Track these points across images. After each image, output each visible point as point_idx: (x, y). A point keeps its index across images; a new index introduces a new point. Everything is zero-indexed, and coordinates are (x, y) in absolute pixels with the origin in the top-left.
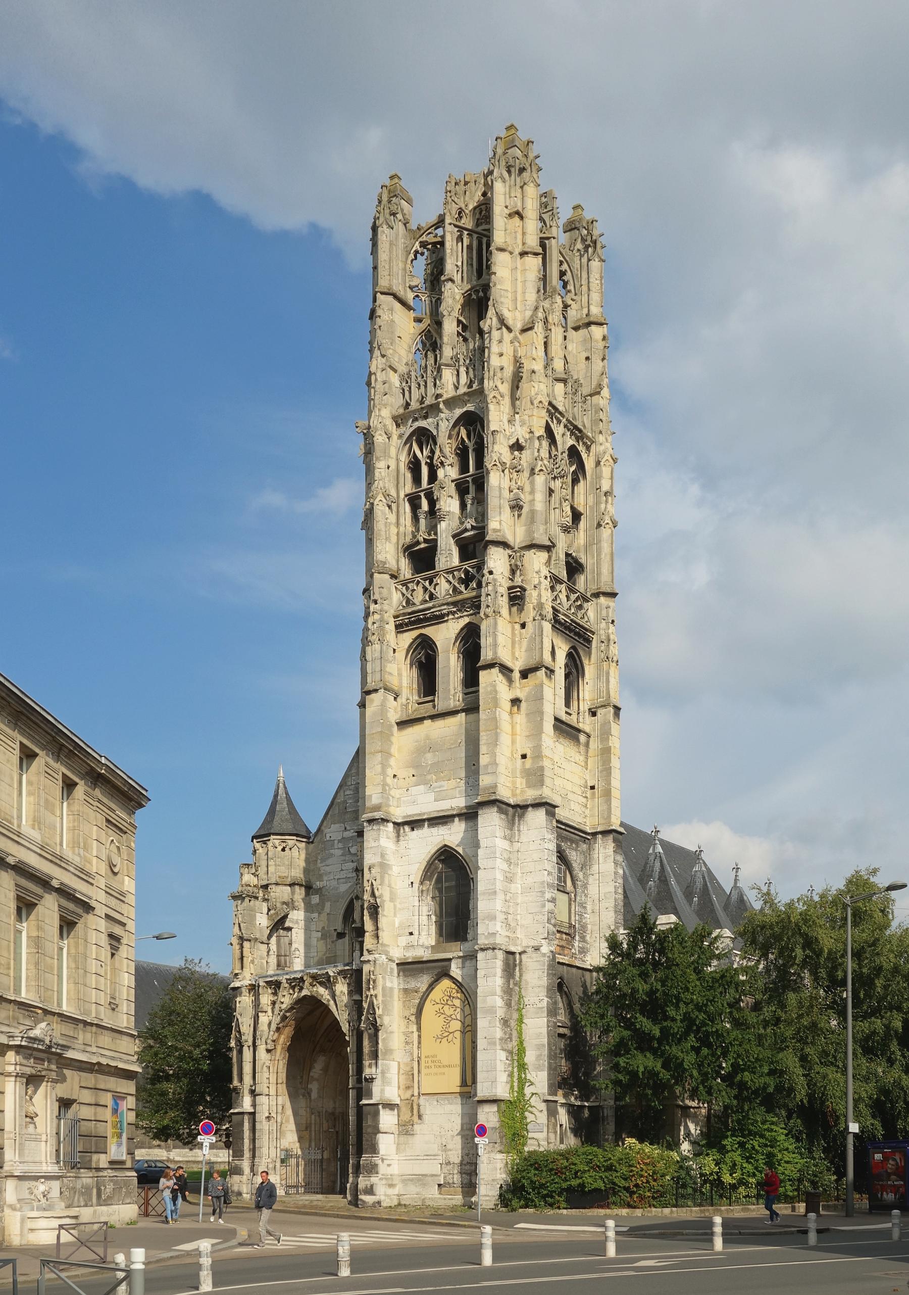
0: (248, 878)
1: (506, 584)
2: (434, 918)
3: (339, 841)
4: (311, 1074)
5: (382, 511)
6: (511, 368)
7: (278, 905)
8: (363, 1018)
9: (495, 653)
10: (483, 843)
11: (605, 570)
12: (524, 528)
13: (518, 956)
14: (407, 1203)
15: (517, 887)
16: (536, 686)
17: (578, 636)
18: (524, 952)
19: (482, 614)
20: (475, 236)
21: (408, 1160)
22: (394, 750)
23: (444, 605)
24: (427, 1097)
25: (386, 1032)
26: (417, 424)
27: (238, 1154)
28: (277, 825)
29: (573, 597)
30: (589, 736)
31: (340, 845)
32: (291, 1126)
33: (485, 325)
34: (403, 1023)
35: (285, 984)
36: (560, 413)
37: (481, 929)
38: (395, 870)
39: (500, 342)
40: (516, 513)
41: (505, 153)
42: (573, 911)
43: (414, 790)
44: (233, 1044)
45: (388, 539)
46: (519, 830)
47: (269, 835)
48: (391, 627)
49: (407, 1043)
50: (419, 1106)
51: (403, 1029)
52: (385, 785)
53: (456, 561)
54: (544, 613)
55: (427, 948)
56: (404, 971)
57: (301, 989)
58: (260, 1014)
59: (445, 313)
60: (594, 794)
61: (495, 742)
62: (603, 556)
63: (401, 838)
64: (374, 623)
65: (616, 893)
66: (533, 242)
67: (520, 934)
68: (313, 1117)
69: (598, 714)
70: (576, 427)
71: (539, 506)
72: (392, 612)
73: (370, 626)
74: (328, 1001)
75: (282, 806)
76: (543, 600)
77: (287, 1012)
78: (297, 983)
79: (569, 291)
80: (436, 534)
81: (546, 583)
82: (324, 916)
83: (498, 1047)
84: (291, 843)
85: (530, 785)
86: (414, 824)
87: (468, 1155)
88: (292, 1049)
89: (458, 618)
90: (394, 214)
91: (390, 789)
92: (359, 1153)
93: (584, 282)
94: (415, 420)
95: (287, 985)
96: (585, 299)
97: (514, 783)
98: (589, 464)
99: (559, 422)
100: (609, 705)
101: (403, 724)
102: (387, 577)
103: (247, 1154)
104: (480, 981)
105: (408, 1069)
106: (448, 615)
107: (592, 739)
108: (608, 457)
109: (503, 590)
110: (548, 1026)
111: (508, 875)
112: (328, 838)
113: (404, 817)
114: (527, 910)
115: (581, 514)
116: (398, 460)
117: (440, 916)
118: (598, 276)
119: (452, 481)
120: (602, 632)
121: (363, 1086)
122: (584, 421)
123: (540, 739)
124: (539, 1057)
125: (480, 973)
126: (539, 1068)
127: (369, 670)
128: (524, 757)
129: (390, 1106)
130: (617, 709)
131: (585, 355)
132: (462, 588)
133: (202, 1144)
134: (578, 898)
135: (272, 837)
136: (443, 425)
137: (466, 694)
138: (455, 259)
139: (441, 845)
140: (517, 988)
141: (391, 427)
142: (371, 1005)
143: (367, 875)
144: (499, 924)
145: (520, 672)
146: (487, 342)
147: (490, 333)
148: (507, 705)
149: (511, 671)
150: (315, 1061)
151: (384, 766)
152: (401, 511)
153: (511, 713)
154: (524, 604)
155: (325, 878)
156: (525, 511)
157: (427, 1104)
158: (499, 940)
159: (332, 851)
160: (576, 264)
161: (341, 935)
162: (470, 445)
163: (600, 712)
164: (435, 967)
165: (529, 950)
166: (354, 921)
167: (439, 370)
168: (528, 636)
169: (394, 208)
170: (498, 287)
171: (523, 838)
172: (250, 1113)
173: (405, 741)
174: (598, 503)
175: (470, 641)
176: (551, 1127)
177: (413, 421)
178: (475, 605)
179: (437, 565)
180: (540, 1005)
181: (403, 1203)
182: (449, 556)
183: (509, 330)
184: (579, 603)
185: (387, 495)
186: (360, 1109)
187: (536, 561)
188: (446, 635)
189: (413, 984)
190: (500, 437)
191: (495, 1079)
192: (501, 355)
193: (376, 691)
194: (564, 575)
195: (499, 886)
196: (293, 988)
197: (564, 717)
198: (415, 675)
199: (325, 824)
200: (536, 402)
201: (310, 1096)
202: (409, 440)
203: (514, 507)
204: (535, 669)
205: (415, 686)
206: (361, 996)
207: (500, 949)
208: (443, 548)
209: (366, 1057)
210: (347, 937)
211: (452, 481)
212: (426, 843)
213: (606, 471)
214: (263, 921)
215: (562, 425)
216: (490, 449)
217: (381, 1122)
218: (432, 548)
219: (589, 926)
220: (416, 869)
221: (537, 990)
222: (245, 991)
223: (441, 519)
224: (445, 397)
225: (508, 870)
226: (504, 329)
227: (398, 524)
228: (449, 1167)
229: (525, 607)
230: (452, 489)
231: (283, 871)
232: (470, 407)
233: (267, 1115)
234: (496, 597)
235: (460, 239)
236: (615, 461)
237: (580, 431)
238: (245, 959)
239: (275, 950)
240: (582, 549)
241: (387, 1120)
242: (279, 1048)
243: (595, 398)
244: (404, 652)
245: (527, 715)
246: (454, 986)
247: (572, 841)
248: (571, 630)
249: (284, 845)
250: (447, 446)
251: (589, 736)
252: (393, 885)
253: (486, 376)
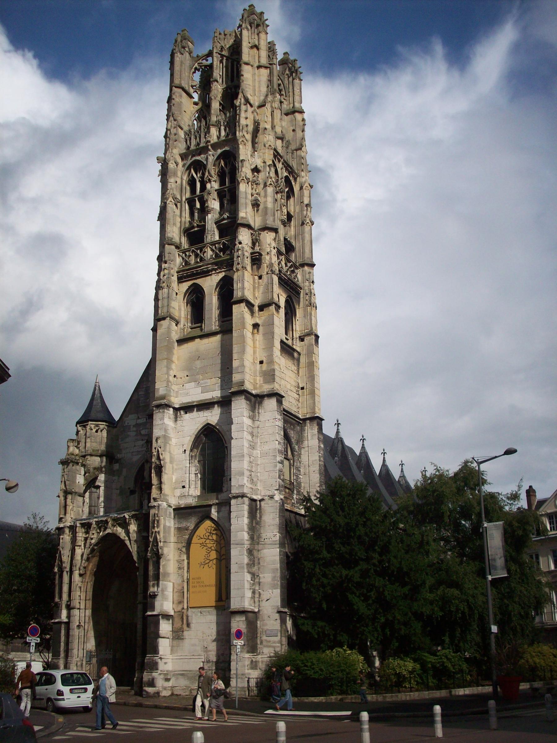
0: (73, 449)
1: (250, 251)
2: (199, 475)
3: (134, 426)
5: (171, 208)
6: (252, 126)
7: (91, 470)
8: (149, 549)
9: (243, 293)
10: (235, 420)
11: (307, 251)
12: (260, 218)
13: (258, 503)
14: (178, 693)
15: (257, 453)
17: (292, 289)
19: (234, 269)
20: (230, 61)
21: (178, 659)
22: (175, 358)
25: (165, 559)
26: (194, 158)
27: (56, 655)
28: (93, 415)
31: (135, 429)
32: (91, 634)
33: (237, 102)
34: (177, 553)
35: (94, 525)
36: (280, 156)
37: (233, 482)
38: (173, 441)
39: (246, 111)
41: (248, 17)
42: (292, 473)
43: (187, 386)
44: (56, 570)
45: (174, 224)
46: (259, 413)
47: (88, 421)
48: (175, 278)
49: (180, 568)
50: (187, 616)
51: (177, 558)
52: (168, 381)
53: (217, 238)
54: (274, 269)
55: (195, 497)
56: (178, 514)
57: (105, 529)
58: (76, 547)
59: (213, 98)
60: (303, 393)
61: (243, 351)
62: (306, 242)
63: (178, 419)
64: (164, 275)
65: (320, 460)
66: (264, 61)
67: (259, 486)
70: (289, 165)
71: (270, 205)
72: (176, 269)
73: (161, 277)
75: (97, 402)
76: (273, 262)
77: (95, 545)
78: (103, 525)
79: (283, 95)
80: (205, 222)
81: (274, 251)
83: (246, 570)
84: (102, 427)
85: (266, 381)
86: (188, 408)
87: (223, 655)
89: (218, 273)
90: (184, 48)
91: (172, 385)
92: (144, 655)
93: (291, 90)
94: (193, 156)
95: (95, 526)
96: (291, 99)
97: (255, 380)
98: (296, 188)
99: (279, 161)
100: (312, 334)
101: (181, 342)
103: (62, 655)
104: (232, 521)
105: (180, 588)
106: (212, 270)
107: (301, 356)
108: (307, 184)
109: (247, 254)
111: (252, 444)
112: (126, 424)
113: (181, 404)
114: (265, 470)
115: (292, 217)
116: (182, 179)
117: (203, 474)
119: (216, 191)
120: (306, 288)
121: (149, 600)
122: (294, 164)
123: (273, 351)
124: (274, 578)
125: (233, 515)
127: (160, 305)
128: (261, 362)
129: (167, 617)
131: (292, 128)
134: (295, 464)
135: (90, 422)
136: (210, 158)
137: (223, 322)
138: (218, 72)
141: (179, 160)
143: (154, 444)
144: (246, 479)
145: (259, 307)
146: (238, 111)
147: (240, 106)
148: (250, 328)
151: (169, 368)
152: (184, 209)
153: (253, 333)
154: (261, 264)
156: (261, 207)
157: (194, 616)
158: (246, 490)
159: (129, 433)
160: (286, 82)
161: (132, 492)
162: (227, 170)
164: (199, 512)
165: (267, 498)
167: (209, 129)
169: (184, 44)
170: (245, 82)
171: (261, 418)
172: (65, 623)
173: (181, 353)
174: (302, 210)
175: (226, 290)
176: (283, 632)
177: (192, 157)
178: (229, 265)
179: (205, 240)
181: (175, 693)
182: (213, 234)
183: (251, 106)
184: (292, 269)
185: (175, 198)
186: (145, 618)
187: (268, 238)
188: (210, 284)
189: (184, 524)
190: (246, 164)
191: (242, 597)
192: (246, 118)
193: (164, 319)
194: (283, 250)
195: (246, 451)
196: (100, 528)
197: (285, 340)
198: (189, 310)
200: (267, 146)
202: (189, 168)
205: (189, 317)
206: (148, 532)
207: (247, 497)
208: (209, 229)
209: (151, 579)
212: (194, 422)
213: (306, 193)
214: (80, 480)
215: (281, 163)
216: (240, 170)
217: (161, 628)
218: (203, 230)
219: (302, 484)
220: (188, 441)
221: (272, 527)
222: (67, 530)
223: (209, 212)
224: (212, 142)
225: (251, 440)
226: (248, 105)
227: (181, 216)
230: (215, 195)
231: (95, 446)
232: (227, 148)
233: (78, 624)
234: (243, 258)
235: (221, 62)
237: (291, 168)
238: (67, 507)
240: (293, 238)
241: (165, 627)
242: (88, 573)
243: (299, 152)
245: (264, 334)
246: (213, 525)
247: (291, 424)
248: (288, 285)
249: (97, 428)
250: (212, 170)
251: (299, 354)
252: (172, 452)
253: (238, 129)
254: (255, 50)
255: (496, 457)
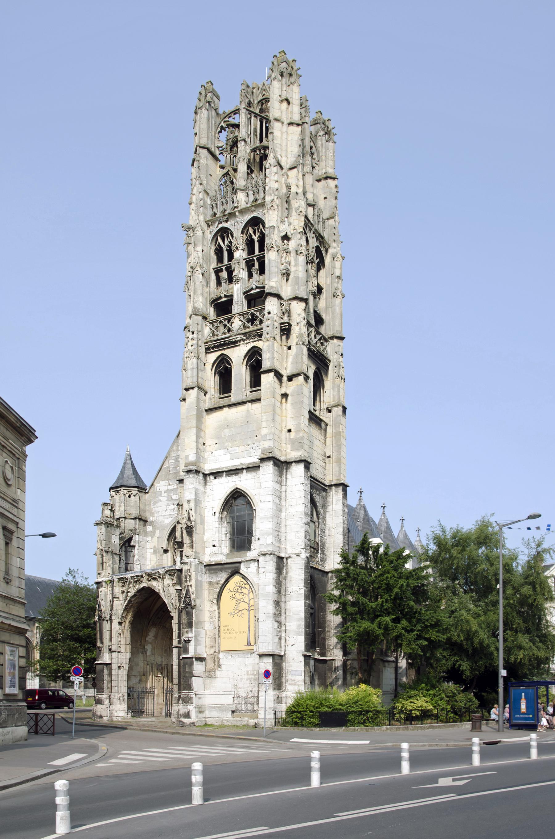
3: (165, 492)
4: (147, 639)
13: (285, 560)
16: (298, 386)
17: (320, 361)
18: (290, 557)
23: (237, 335)
24: (224, 653)
26: (220, 226)
29: (318, 337)
30: (327, 425)
31: (166, 494)
36: (311, 224)
40: (285, 278)
46: (286, 478)
56: (209, 570)
63: (208, 484)
64: (192, 346)
68: (148, 667)
69: (333, 411)
74: (159, 590)
82: (155, 539)
86: (216, 474)
88: (134, 625)
89: (247, 343)
91: (201, 452)
94: (221, 222)
99: (310, 230)
101: (209, 411)
102: (200, 318)
105: (212, 634)
106: (240, 341)
110: (305, 606)
111: (279, 506)
112: (158, 490)
113: (210, 470)
115: (322, 289)
118: (331, 151)
119: (244, 259)
126: (298, 634)
130: (344, 409)
132: (249, 324)
133: (73, 682)
134: (320, 526)
135: (122, 488)
136: (236, 226)
139: (234, 488)
140: (284, 581)
142: (188, 591)
149: (282, 376)
150: (149, 631)
155: (156, 515)
159: (160, 498)
161: (166, 551)
163: (334, 410)
166: (175, 538)
168: (293, 355)
177: (219, 224)
180: (299, 592)
182: (239, 305)
188: (237, 355)
193: (193, 388)
197: (313, 411)
199: (156, 481)
201: (146, 654)
203: (284, 274)
204: (298, 375)
210: (170, 551)
211: (244, 259)
215: (312, 232)
225: (279, 503)
228: (239, 699)
229: (291, 337)
236: (343, 258)
237: (322, 238)
239: (124, 559)
244: (211, 365)
245: (292, 404)
249: (130, 493)
250: (239, 240)
254: (285, 104)
255: (519, 521)
